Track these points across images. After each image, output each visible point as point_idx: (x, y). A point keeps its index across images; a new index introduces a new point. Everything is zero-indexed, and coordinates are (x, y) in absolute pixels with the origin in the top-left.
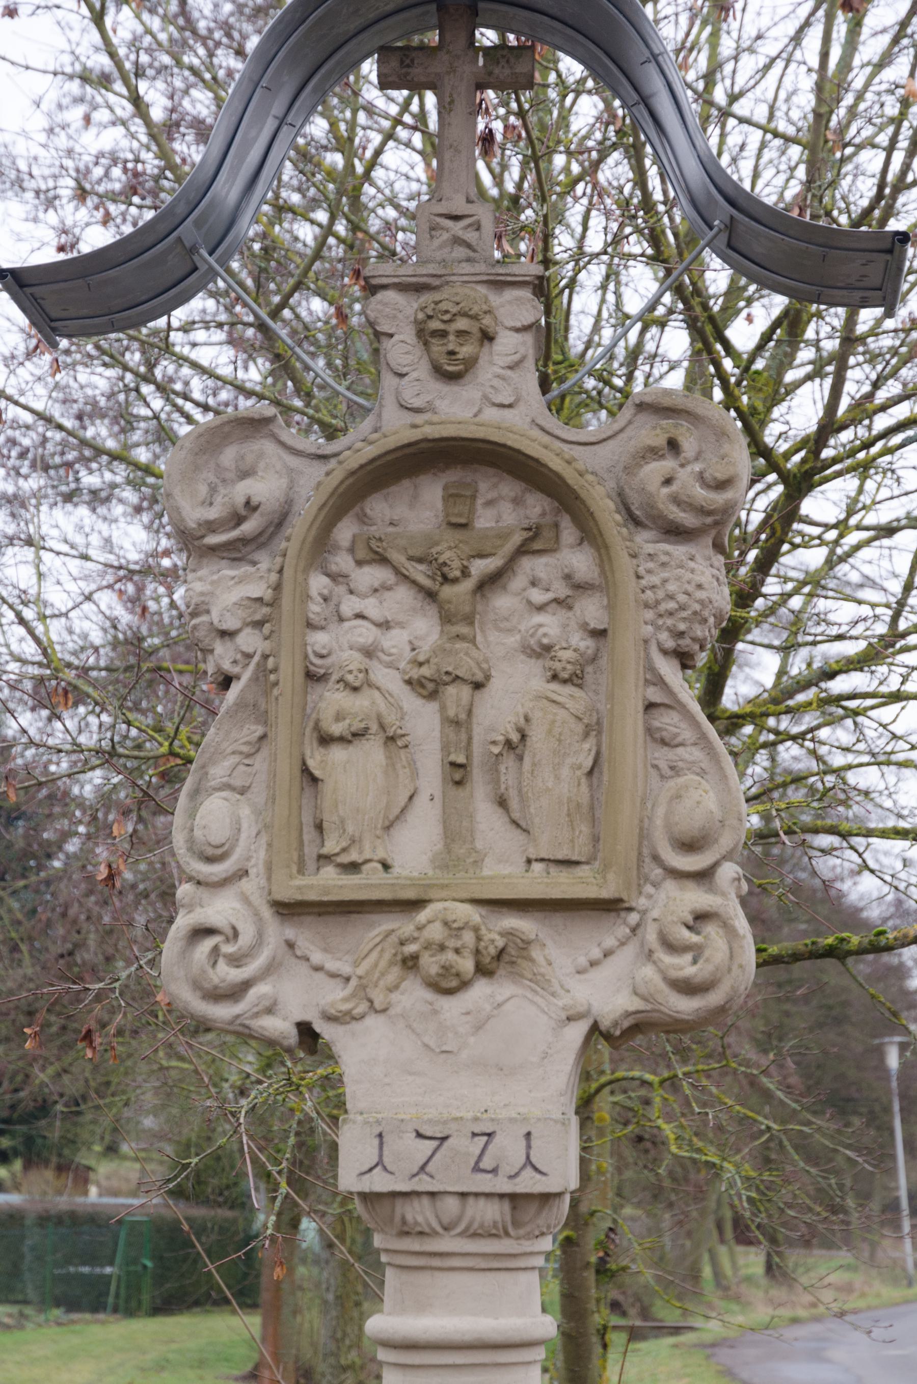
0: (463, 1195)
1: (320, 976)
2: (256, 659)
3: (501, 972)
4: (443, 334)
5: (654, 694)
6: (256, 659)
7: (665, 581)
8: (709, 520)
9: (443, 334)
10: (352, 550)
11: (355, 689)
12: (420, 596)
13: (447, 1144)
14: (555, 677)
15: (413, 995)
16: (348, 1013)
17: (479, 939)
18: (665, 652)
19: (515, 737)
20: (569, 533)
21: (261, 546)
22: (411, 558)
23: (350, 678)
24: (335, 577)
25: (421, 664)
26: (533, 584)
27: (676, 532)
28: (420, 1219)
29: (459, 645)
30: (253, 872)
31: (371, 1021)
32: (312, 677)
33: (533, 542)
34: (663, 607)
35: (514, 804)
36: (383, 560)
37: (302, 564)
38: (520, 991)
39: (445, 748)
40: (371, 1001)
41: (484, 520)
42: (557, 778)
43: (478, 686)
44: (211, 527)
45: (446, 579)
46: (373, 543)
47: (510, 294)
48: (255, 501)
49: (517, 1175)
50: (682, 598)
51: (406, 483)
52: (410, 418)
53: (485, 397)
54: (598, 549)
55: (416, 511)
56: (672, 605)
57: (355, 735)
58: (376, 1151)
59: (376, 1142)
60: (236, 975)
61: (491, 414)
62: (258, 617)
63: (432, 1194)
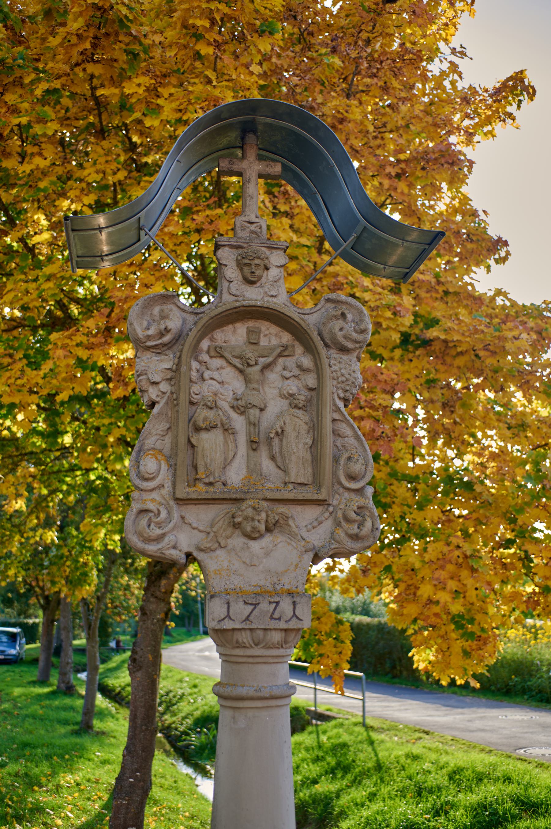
0: (265, 630)
1: (196, 531)
2: (168, 394)
3: (276, 531)
4: (249, 265)
5: (336, 416)
6: (168, 394)
7: (341, 369)
8: (358, 346)
9: (249, 265)
10: (208, 352)
11: (211, 408)
12: (237, 372)
13: (258, 607)
14: (296, 407)
15: (238, 541)
16: (209, 548)
17: (267, 516)
18: (340, 398)
19: (280, 431)
20: (299, 349)
21: (169, 348)
22: (233, 356)
23: (209, 404)
24: (200, 362)
25: (238, 400)
26: (284, 369)
27: (343, 350)
28: (245, 640)
29: (254, 392)
30: (166, 486)
31: (219, 552)
32: (192, 403)
33: (284, 351)
34: (340, 379)
35: (279, 459)
36: (222, 356)
37: (189, 355)
38: (284, 539)
39: (249, 434)
40: (219, 543)
41: (264, 342)
42: (298, 448)
43: (262, 410)
44: (149, 338)
45: (249, 365)
46: (218, 349)
47: (276, 252)
48: (169, 327)
49: (290, 620)
50: (347, 376)
51: (231, 326)
53: (265, 293)
54: (314, 355)
55: (235, 336)
56: (344, 379)
57: (212, 427)
58: (225, 609)
59: (226, 606)
60: (159, 532)
62: (169, 377)
63: (251, 630)
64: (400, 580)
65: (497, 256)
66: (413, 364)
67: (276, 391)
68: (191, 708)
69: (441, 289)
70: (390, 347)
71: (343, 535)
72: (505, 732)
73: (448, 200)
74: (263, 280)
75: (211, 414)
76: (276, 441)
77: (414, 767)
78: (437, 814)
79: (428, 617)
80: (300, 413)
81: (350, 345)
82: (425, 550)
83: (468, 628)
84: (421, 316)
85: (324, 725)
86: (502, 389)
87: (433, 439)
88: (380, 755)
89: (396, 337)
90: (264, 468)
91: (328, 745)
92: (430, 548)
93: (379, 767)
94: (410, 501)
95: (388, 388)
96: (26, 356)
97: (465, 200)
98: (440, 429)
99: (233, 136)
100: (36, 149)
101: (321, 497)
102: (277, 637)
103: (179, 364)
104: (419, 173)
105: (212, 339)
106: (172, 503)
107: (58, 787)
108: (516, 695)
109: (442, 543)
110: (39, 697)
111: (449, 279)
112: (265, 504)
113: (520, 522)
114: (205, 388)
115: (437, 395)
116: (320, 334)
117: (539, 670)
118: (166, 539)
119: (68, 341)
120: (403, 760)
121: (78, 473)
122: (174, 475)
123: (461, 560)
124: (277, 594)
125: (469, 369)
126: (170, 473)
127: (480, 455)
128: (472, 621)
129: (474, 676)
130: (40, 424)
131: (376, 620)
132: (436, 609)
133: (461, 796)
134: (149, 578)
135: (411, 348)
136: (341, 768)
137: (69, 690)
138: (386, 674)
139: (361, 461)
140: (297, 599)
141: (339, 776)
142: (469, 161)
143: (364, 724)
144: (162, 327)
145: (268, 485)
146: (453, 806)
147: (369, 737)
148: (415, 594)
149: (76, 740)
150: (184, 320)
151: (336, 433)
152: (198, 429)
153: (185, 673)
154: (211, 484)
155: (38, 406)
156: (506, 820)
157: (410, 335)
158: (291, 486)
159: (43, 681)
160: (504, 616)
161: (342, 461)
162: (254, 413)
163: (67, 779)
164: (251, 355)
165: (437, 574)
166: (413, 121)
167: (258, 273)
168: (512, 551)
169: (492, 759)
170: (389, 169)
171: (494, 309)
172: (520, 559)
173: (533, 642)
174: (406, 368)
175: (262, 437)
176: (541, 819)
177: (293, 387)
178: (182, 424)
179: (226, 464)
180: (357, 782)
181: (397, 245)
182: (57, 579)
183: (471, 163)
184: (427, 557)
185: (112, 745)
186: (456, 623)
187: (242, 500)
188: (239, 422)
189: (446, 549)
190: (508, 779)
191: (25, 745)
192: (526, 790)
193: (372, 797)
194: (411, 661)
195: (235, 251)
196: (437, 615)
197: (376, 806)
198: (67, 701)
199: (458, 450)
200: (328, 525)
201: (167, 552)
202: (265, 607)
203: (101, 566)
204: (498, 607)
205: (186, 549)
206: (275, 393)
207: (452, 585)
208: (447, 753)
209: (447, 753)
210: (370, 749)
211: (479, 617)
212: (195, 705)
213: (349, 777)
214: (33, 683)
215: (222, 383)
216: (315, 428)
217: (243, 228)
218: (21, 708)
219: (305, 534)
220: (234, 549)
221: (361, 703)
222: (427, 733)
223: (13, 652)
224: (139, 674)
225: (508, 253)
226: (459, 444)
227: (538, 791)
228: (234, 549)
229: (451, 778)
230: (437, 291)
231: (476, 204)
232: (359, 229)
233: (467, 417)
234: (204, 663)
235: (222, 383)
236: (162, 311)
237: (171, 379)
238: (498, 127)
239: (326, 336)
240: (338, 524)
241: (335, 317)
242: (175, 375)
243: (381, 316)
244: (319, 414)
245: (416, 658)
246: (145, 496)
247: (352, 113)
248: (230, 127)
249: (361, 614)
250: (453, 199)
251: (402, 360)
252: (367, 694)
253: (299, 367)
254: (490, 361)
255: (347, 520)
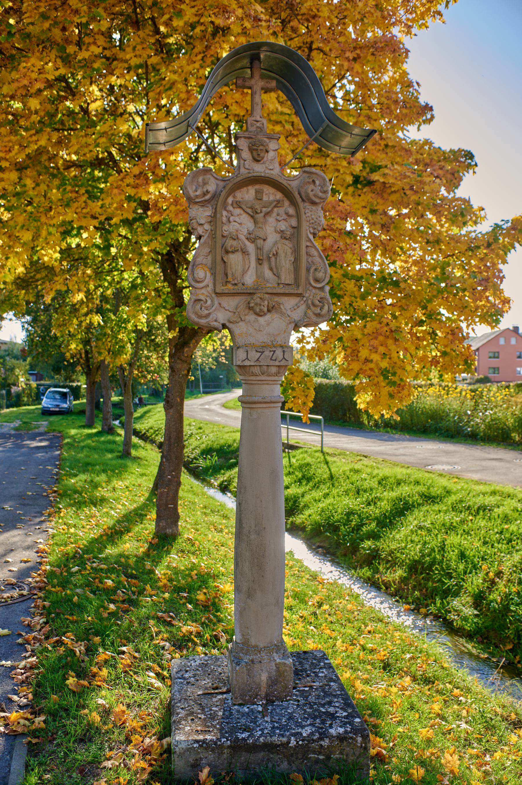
5: (309, 244)
9: (257, 150)
10: (232, 205)
14: (285, 238)
15: (251, 317)
20: (287, 203)
24: (228, 211)
27: (313, 203)
31: (241, 323)
32: (223, 236)
33: (278, 204)
35: (274, 270)
36: (240, 207)
39: (257, 255)
41: (265, 198)
43: (264, 240)
44: (197, 196)
45: (257, 213)
52: (247, 171)
55: (248, 194)
60: (207, 312)
61: (267, 171)
64: (348, 347)
65: (424, 118)
66: (361, 198)
67: (273, 229)
68: (198, 443)
69: (383, 143)
70: (345, 185)
71: (311, 314)
72: (419, 456)
73: (391, 74)
74: (265, 159)
75: (235, 243)
76: (273, 259)
77: (355, 477)
78: (369, 504)
79: (366, 370)
80: (287, 242)
81: (317, 200)
82: (365, 326)
83: (391, 379)
84: (368, 163)
85: (293, 453)
86: (422, 216)
87: (374, 252)
88: (332, 470)
89: (349, 179)
90: (266, 275)
91: (297, 464)
92: (368, 325)
93: (331, 477)
94: (356, 294)
95: (343, 216)
96: (87, 192)
97: (405, 74)
98: (379, 243)
99: (246, 62)
100: (91, 40)
101: (300, 291)
102: (274, 370)
103: (215, 213)
104: (370, 58)
105: (234, 197)
106: (214, 295)
107: (114, 489)
108: (431, 433)
109: (376, 322)
110: (90, 436)
111: (389, 136)
112: (267, 296)
113: (429, 309)
114: (231, 227)
115: (377, 218)
116: (299, 193)
117: (448, 415)
118: (211, 316)
119: (120, 183)
120: (348, 473)
121: (116, 273)
122: (215, 280)
123: (388, 333)
124: (274, 347)
125: (399, 203)
126: (212, 278)
127: (406, 262)
128: (394, 374)
129: (397, 412)
130: (98, 240)
131: (332, 382)
132: (372, 365)
133: (385, 493)
134: (176, 346)
135: (359, 186)
136: (306, 479)
137: (111, 431)
138: (339, 420)
139: (323, 271)
140: (285, 349)
141: (304, 483)
142: (406, 49)
143: (322, 451)
144: (205, 190)
145: (268, 285)
146: (379, 499)
147: (325, 459)
148: (357, 356)
149: (120, 461)
150: (217, 185)
151: (308, 254)
152: (227, 252)
153: (192, 420)
154: (235, 284)
155: (95, 227)
156: (414, 506)
157: (359, 177)
158: (281, 286)
159: (90, 425)
160: (417, 371)
161: (312, 271)
162: (260, 242)
163: (119, 484)
164: (258, 207)
165: (372, 343)
166: (367, 15)
167: (262, 155)
168: (424, 328)
169: (409, 471)
170: (348, 54)
171: (422, 154)
172: (429, 333)
173: (445, 396)
174: (356, 201)
175: (265, 256)
176: (436, 505)
177: (283, 226)
178: (219, 250)
179: (244, 272)
180: (316, 487)
181: (346, 136)
182: (102, 351)
183: (407, 51)
184: (366, 331)
185: (145, 465)
186: (384, 375)
187: (254, 294)
188: (251, 247)
189: (378, 326)
190: (417, 483)
191: (88, 464)
192: (428, 489)
193: (326, 496)
194: (355, 403)
195: (247, 140)
196: (371, 369)
197: (328, 501)
198: (110, 437)
199: (391, 259)
200: (303, 307)
201: (212, 324)
202: (267, 353)
203: (133, 341)
204: (413, 366)
205: (222, 322)
206: (272, 229)
207: (382, 349)
208: (378, 468)
209: (378, 468)
210: (325, 466)
211: (399, 372)
212: (201, 441)
213: (311, 484)
214: (84, 427)
215: (240, 224)
216: (296, 251)
217: (252, 125)
218: (79, 442)
219: (289, 313)
220: (249, 322)
221: (319, 438)
222: (366, 457)
223: (65, 406)
224: (171, 411)
225: (433, 117)
226: (391, 254)
227: (436, 489)
228: (249, 322)
229: (379, 483)
230: (380, 145)
231: (413, 77)
232: (324, 125)
233: (398, 235)
234: (205, 413)
235: (240, 224)
236: (204, 179)
237: (210, 222)
238: (429, 20)
239: (303, 194)
240: (308, 308)
241: (309, 182)
242: (214, 219)
243: (340, 165)
244: (298, 243)
245: (358, 402)
246: (198, 291)
247: (322, 11)
248: (244, 57)
249: (322, 377)
250: (395, 73)
251: (353, 195)
252: (325, 433)
253: (287, 214)
254: (414, 198)
255: (314, 305)
